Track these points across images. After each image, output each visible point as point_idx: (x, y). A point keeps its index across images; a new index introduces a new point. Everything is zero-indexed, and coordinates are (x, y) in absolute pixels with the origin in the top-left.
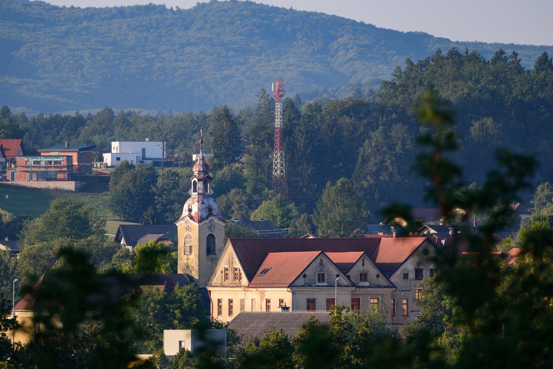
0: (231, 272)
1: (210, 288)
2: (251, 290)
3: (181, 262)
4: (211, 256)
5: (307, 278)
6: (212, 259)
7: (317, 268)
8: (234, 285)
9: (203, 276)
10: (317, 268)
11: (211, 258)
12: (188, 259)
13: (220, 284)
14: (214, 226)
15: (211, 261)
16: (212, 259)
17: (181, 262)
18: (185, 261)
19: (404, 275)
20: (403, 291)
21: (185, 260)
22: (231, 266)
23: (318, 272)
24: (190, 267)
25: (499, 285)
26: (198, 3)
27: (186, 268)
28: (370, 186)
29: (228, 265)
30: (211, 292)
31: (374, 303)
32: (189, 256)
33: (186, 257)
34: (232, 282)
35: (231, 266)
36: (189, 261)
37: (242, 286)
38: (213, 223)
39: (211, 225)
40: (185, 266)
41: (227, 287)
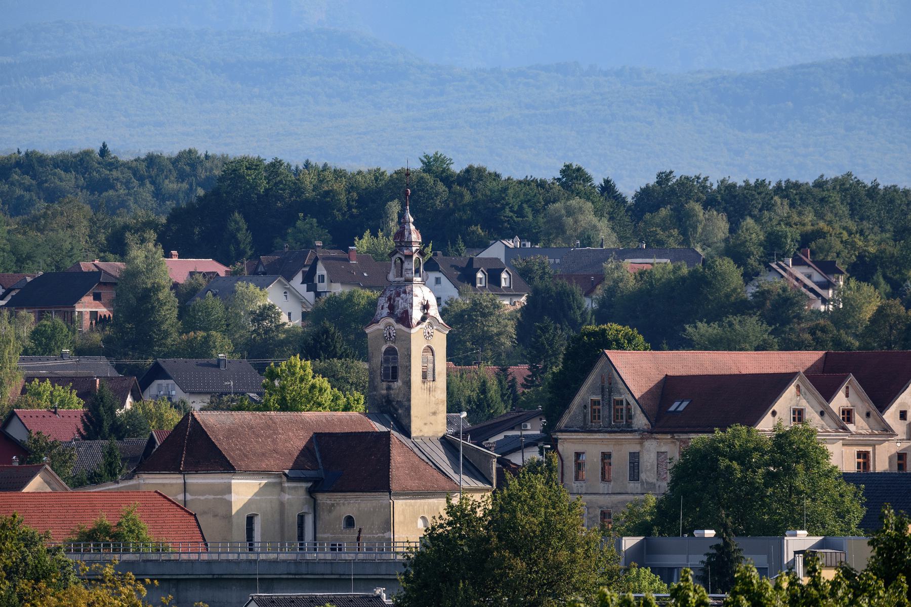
0: (607, 407)
1: (558, 434)
2: (659, 437)
3: (375, 393)
4: (428, 383)
5: (777, 417)
6: (430, 388)
7: (791, 400)
8: (616, 429)
9: (417, 417)
10: (791, 401)
11: (428, 387)
12: (389, 388)
13: (582, 428)
14: (394, 334)
15: (428, 392)
16: (430, 388)
17: (375, 393)
18: (384, 392)
19: (901, 412)
20: (900, 440)
21: (382, 390)
22: (606, 396)
23: (794, 407)
24: (393, 401)
25: (675, 466)
26: (663, 178)
27: (385, 404)
28: (515, 247)
29: (600, 396)
30: (559, 441)
31: (815, 473)
32: (390, 384)
33: (385, 385)
34: (610, 423)
35: (606, 396)
36: (392, 392)
37: (635, 431)
38: (393, 329)
39: (390, 334)
40: (384, 400)
41: (599, 432)
